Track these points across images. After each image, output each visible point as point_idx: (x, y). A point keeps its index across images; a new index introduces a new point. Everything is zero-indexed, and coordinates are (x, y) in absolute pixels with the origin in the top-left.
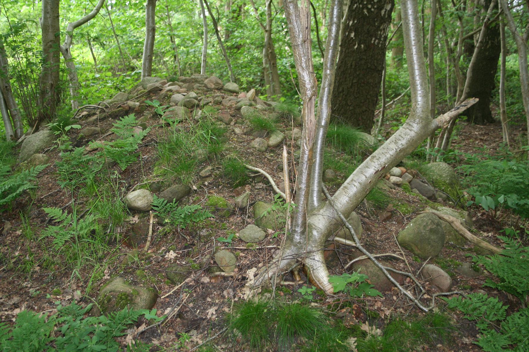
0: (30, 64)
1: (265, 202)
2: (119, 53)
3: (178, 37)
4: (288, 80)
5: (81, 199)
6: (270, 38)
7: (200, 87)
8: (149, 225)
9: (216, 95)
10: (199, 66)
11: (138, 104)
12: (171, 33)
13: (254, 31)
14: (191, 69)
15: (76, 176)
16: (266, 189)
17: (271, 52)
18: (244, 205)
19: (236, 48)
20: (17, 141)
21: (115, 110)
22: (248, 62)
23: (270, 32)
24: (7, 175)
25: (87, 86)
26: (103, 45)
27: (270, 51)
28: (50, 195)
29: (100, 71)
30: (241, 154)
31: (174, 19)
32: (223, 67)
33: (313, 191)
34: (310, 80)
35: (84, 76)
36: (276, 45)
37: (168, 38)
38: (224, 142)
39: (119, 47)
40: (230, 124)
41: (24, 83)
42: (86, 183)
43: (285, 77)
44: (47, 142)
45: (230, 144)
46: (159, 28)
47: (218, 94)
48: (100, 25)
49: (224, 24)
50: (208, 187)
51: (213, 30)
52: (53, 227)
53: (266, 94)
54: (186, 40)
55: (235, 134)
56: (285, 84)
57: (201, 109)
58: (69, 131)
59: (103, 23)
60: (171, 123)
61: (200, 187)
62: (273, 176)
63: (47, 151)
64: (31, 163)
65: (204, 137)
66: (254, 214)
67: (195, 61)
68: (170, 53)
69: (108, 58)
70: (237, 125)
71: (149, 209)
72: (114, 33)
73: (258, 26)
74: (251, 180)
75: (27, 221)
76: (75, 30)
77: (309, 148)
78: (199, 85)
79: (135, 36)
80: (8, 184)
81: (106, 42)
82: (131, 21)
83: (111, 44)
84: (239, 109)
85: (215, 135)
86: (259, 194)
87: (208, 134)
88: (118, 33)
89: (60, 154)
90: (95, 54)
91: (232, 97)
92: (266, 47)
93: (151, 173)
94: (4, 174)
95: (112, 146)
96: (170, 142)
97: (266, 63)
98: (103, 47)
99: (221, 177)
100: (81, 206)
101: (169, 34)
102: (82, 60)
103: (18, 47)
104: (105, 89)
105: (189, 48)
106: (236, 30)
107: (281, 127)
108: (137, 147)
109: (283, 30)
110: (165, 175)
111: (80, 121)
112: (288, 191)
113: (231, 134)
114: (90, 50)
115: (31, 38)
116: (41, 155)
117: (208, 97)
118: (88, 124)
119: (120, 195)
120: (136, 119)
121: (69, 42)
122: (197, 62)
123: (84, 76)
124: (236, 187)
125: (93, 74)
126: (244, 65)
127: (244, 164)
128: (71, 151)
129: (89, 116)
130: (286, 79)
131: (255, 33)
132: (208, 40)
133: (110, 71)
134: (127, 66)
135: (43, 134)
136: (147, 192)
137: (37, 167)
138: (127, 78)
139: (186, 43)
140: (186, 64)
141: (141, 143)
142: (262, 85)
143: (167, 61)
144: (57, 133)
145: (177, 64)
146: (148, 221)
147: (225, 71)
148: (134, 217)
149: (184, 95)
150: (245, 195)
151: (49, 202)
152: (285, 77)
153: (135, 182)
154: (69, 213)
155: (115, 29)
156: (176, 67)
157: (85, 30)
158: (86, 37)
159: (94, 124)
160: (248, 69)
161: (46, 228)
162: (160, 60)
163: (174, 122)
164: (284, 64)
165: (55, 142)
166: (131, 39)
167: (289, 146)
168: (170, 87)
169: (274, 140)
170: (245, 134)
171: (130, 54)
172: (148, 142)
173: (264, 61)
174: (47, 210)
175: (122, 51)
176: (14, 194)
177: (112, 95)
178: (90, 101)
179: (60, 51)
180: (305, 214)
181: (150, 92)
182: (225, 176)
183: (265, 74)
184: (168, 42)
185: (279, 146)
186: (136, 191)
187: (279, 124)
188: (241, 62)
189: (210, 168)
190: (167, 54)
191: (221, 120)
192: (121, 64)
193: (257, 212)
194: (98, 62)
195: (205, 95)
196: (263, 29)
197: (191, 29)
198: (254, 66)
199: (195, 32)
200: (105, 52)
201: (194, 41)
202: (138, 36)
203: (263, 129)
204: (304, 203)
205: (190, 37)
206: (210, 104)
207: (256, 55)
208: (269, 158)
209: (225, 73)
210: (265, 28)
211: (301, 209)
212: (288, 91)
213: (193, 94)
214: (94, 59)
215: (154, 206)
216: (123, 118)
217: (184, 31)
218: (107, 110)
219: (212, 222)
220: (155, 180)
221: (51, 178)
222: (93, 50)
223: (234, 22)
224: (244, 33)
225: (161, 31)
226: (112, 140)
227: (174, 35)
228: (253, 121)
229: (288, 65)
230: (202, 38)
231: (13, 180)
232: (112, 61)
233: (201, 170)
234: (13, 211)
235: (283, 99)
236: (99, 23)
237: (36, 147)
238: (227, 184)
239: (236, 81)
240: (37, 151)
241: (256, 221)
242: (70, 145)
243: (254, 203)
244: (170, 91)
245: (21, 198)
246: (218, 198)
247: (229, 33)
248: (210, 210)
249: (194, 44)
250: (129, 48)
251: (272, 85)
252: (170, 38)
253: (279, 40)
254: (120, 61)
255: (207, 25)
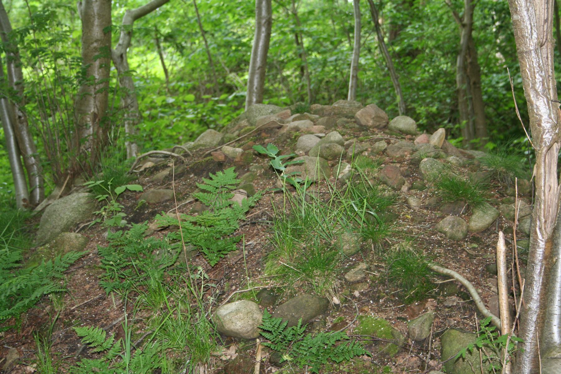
0: (60, 79)
1: (462, 330)
2: (207, 62)
3: (309, 35)
4: (500, 110)
5: (139, 313)
6: (470, 38)
7: (347, 122)
8: (254, 364)
9: (375, 137)
10: (345, 85)
11: (240, 150)
12: (298, 29)
13: (441, 26)
14: (329, 91)
15: (130, 273)
16: (464, 308)
17: (471, 63)
18: (424, 336)
19: (409, 54)
20: (33, 209)
21: (201, 160)
22: (429, 80)
23: (471, 27)
24: (15, 268)
25: (152, 118)
26: (180, 49)
27: (469, 60)
28: (85, 305)
29: (174, 92)
30: (420, 243)
31: (303, 5)
32: (386, 89)
33: (551, 314)
34: (549, 115)
35: (148, 100)
36: (480, 50)
37: (291, 37)
38: (389, 221)
39: (208, 52)
40: (400, 189)
41: (48, 111)
42: (148, 286)
43: (495, 106)
44: (84, 212)
45: (400, 225)
46: (277, 20)
47: (379, 136)
48: (177, 15)
49: (388, 14)
50: (359, 300)
51: (369, 23)
52: (90, 361)
53: (460, 136)
54: (321, 40)
55: (409, 208)
56: (495, 120)
57: (348, 162)
58: (121, 195)
59: (181, 11)
60: (297, 186)
61: (346, 301)
62: (477, 285)
63: (83, 228)
64: (59, 247)
65: (353, 211)
66: (442, 351)
67: (335, 77)
68: (293, 62)
69: (188, 69)
70: (413, 191)
71: (256, 335)
72: (201, 27)
73: (449, 17)
74: (437, 290)
75: (46, 349)
76: (135, 23)
77: (546, 237)
78: (345, 119)
79: (234, 34)
80: (17, 282)
81: (186, 42)
82: (229, 8)
83: (194, 46)
84: (415, 163)
85: (373, 207)
86: (451, 317)
87: (362, 207)
88: (207, 28)
89: (106, 234)
90: (167, 63)
91: (404, 142)
92: (463, 54)
93: (260, 272)
94: (11, 265)
95: (195, 223)
96: (295, 218)
97: (462, 82)
98: (181, 52)
99: (382, 282)
100: (138, 326)
101: (293, 31)
102: (144, 73)
103: (43, 50)
104: (183, 124)
105: (328, 55)
106: (410, 24)
107: (492, 196)
108: (238, 227)
109: (494, 23)
110: (285, 275)
111: (141, 179)
112: (505, 313)
113: (401, 207)
114: (158, 57)
115: (62, 38)
116: (73, 235)
117: (361, 141)
118: (155, 183)
119: (206, 309)
120: (237, 178)
121: (126, 42)
122: (340, 77)
123: (148, 100)
124: (410, 303)
125: (163, 97)
126: (423, 84)
127: (425, 262)
128: (124, 229)
129: (156, 169)
130: (495, 110)
131: (443, 28)
132: (362, 42)
133: (192, 93)
134: (220, 84)
135: (79, 199)
136: (253, 306)
137: (66, 255)
138: (221, 105)
139: (322, 45)
140: (321, 81)
141: (244, 218)
142: (454, 120)
143: (288, 76)
144: (102, 197)
145: (306, 82)
146: (252, 357)
147: (389, 95)
148: (228, 348)
149: (320, 137)
150: (425, 317)
151: (84, 318)
152: (495, 106)
153: (232, 286)
154: (117, 337)
155: (202, 20)
156: (303, 86)
157: (152, 23)
158: (153, 34)
159: (163, 183)
160: (430, 93)
161: (78, 363)
162: (277, 74)
163: (302, 184)
164: (494, 83)
165: (98, 212)
166: (228, 38)
167: (508, 231)
168: (296, 123)
169: (480, 219)
170: (427, 208)
171: (225, 64)
172: (258, 217)
173: (458, 77)
174: (80, 331)
175: (213, 59)
176: (26, 301)
177: (193, 133)
178: (157, 143)
179: (111, 58)
180: (536, 356)
181: (260, 131)
182: (391, 281)
183: (460, 100)
184: (290, 43)
185: (489, 230)
186: (233, 303)
187: (487, 192)
188: (416, 79)
189: (363, 266)
190: (289, 65)
191: (385, 183)
192: (210, 81)
193: (447, 348)
194: (171, 77)
195: (357, 137)
196: (457, 22)
197: (330, 22)
198: (440, 86)
199: (337, 27)
200: (184, 59)
201: (336, 43)
202: (240, 33)
203: (456, 197)
204: (535, 337)
205: (329, 36)
206: (366, 153)
207: (444, 67)
208: (471, 252)
209: (388, 99)
210: (461, 20)
211: (529, 347)
212: (500, 131)
213: (335, 136)
214: (166, 71)
215: (264, 331)
216: (214, 173)
217: (318, 24)
218: (186, 161)
219: (367, 364)
220: (267, 284)
221: (89, 275)
222: (164, 56)
223: (405, 10)
224: (423, 30)
225: (280, 24)
226: (194, 212)
227: (302, 32)
228: (442, 184)
229: (501, 85)
230: (349, 38)
231: (24, 276)
232: (195, 75)
233: (347, 270)
234: (23, 330)
235: (490, 146)
236: (175, 11)
237: (65, 221)
238: (394, 295)
239: (409, 112)
240: (67, 229)
241: (445, 364)
242: (123, 218)
243: (442, 332)
244: (297, 129)
245: (37, 308)
246: (375, 319)
247: (397, 30)
248: (363, 342)
249: (335, 48)
250: (223, 54)
251: (471, 120)
252: (294, 38)
253: (485, 41)
254: (209, 76)
255: (360, 15)
